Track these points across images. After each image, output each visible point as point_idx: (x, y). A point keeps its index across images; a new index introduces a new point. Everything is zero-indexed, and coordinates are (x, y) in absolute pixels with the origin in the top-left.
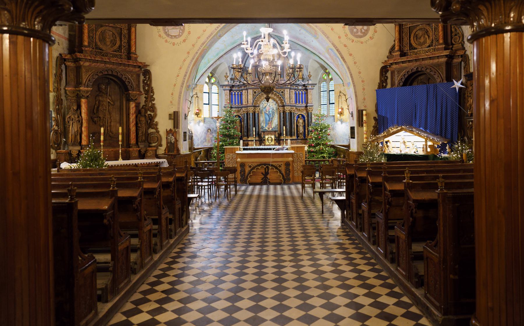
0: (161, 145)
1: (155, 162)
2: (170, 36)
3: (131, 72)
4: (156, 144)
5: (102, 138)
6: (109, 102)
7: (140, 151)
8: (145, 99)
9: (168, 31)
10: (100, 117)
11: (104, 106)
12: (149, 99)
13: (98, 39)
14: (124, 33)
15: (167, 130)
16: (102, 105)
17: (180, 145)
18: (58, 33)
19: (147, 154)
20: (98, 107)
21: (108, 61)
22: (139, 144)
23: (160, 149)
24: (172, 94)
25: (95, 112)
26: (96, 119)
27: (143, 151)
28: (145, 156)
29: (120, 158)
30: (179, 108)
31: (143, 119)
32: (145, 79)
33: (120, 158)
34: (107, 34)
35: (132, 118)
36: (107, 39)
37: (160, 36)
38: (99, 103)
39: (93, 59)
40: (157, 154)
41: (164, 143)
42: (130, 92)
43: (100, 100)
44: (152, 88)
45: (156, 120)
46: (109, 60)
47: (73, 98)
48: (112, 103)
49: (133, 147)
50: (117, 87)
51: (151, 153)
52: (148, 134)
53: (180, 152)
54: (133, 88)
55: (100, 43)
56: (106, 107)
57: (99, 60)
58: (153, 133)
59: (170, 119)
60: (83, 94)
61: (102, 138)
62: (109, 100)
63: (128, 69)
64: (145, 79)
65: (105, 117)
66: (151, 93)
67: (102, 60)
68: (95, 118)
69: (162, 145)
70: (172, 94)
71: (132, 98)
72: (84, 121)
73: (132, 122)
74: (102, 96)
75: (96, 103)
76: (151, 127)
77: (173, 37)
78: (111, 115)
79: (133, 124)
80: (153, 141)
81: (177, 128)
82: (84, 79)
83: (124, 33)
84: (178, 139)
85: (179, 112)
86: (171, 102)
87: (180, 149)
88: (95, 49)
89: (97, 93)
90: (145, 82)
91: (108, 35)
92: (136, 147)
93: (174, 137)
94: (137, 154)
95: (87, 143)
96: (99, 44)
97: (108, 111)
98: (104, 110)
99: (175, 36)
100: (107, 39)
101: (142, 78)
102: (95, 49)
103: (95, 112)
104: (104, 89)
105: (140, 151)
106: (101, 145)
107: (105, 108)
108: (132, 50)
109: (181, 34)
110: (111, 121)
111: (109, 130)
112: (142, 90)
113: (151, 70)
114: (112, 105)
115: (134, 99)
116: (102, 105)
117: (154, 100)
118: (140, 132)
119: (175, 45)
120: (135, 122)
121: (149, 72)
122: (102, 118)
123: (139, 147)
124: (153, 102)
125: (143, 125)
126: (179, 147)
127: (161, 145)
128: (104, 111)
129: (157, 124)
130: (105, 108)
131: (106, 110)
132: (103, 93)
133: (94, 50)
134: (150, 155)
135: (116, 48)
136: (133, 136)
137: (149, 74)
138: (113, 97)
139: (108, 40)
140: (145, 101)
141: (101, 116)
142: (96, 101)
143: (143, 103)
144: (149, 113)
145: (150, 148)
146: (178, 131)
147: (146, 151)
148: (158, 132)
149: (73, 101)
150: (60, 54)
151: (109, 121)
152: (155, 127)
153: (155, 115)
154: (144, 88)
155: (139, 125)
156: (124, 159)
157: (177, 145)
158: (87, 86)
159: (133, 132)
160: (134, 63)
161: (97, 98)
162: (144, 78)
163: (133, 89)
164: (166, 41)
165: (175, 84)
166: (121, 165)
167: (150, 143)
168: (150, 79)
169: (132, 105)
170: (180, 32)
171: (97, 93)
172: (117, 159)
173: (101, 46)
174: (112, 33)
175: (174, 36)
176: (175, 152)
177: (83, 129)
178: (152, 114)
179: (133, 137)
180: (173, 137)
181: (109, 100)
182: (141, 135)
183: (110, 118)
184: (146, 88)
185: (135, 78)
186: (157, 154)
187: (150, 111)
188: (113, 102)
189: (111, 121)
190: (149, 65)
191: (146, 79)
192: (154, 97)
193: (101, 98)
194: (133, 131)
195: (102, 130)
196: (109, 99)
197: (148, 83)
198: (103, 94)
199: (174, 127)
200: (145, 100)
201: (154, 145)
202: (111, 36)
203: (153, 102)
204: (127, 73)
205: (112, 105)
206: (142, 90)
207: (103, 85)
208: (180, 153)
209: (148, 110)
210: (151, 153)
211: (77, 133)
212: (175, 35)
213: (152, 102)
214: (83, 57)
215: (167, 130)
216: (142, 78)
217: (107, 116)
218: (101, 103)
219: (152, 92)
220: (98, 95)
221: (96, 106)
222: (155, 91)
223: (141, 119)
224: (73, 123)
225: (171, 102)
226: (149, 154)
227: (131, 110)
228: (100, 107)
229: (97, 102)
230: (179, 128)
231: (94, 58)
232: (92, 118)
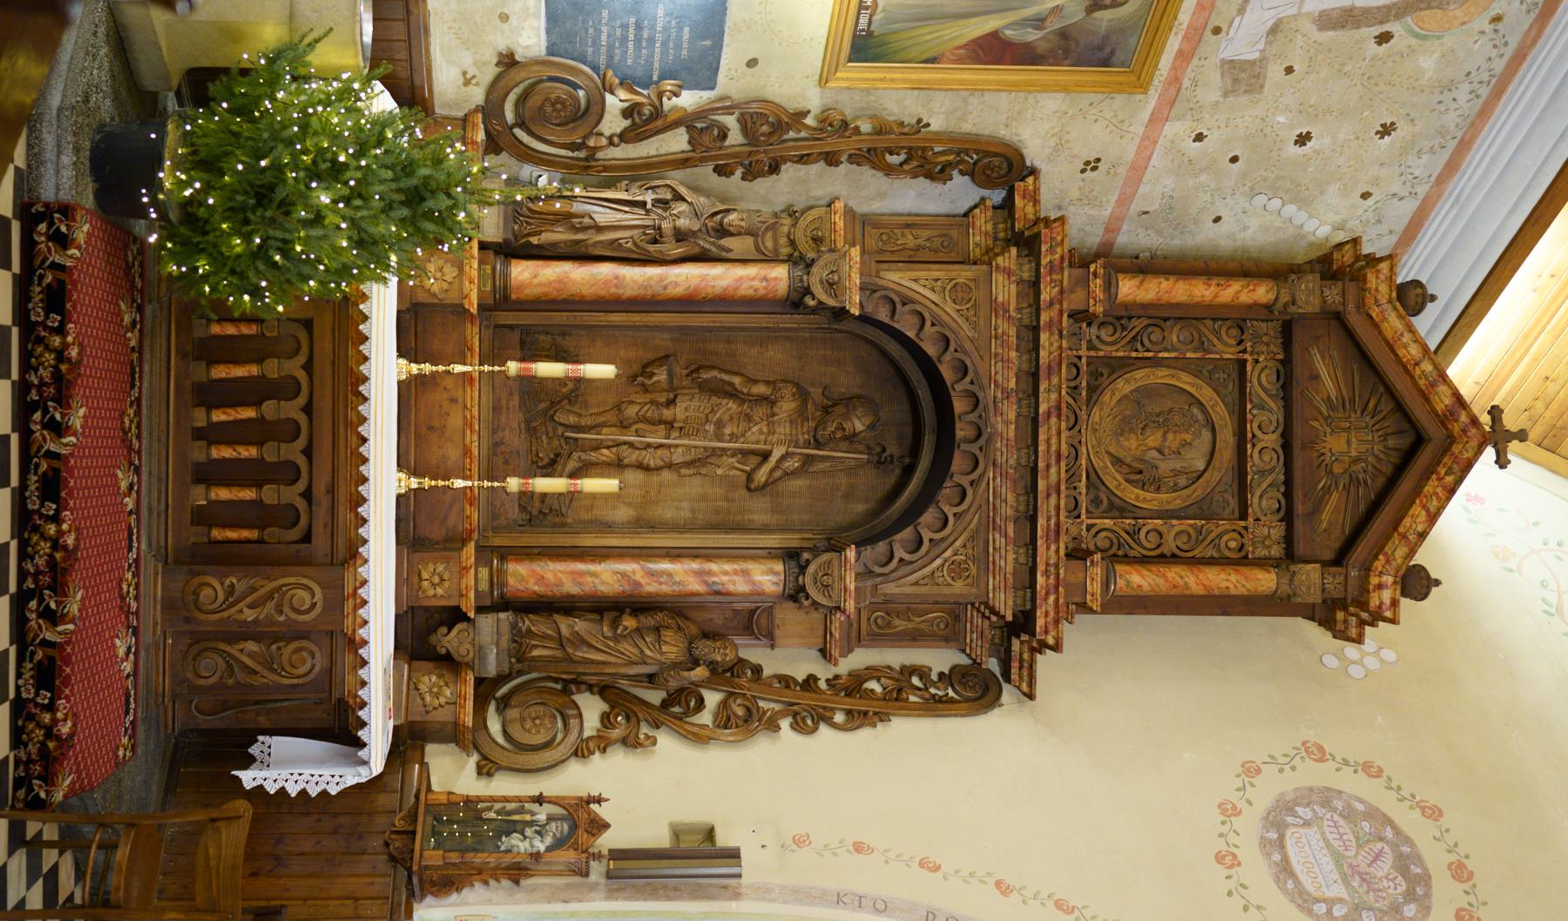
0: (486, 769)
1: (363, 705)
2: (1273, 835)
3: (984, 562)
4: (500, 739)
5: (548, 369)
6: (765, 456)
7: (455, 616)
8: (800, 677)
9: (1307, 824)
10: (671, 403)
11: (743, 425)
12: (807, 699)
13: (1153, 380)
14: (1220, 536)
15: (599, 800)
16: (748, 418)
17: (489, 902)
18: (1153, 162)
19: (430, 673)
20: (732, 394)
21: (1043, 408)
22: (502, 615)
23: (463, 767)
24: (859, 848)
25: (705, 375)
26: (661, 376)
27: (452, 640)
28: (416, 664)
29: (414, 483)
30: (764, 892)
31: (672, 648)
32: (934, 677)
33: (414, 483)
34: (1188, 437)
35: (682, 576)
36: (1159, 435)
37: (1251, 770)
38: (764, 399)
39: (1044, 317)
40: (431, 749)
41: (505, 786)
42: (851, 553)
43: (773, 403)
44: (883, 717)
45: (666, 742)
46: (1049, 414)
47: (783, 241)
48: (762, 475)
49: (484, 573)
50: (860, 508)
51: (437, 695)
52: (566, 692)
53: (429, 900)
54: (877, 570)
55: (1125, 396)
56: (733, 437)
57: (1043, 354)
58: (574, 722)
59: (677, 832)
60: (821, 263)
61: (548, 369)
62: (777, 453)
63: (1000, 541)
64: (934, 677)
65: (676, 434)
66: (849, 712)
67: (1042, 374)
68: (670, 374)
69: (489, 775)
70: (859, 848)
71: (811, 569)
72: (652, 272)
73: (651, 574)
74: (802, 413)
75: (756, 382)
76: (613, 707)
77: (1277, 857)
78: (684, 471)
79: (639, 577)
80: (522, 720)
81: (609, 875)
82: (914, 274)
83: (1220, 536)
84: (534, 889)
85: (736, 895)
86: (800, 841)
87: (454, 897)
88: (1090, 359)
89: (816, 392)
90: (915, 681)
91: (1185, 444)
92: (484, 586)
93: (549, 849)
94: (436, 588)
95: (521, 287)
96: (1123, 387)
97: (714, 452)
98: (720, 424)
99: (1285, 869)
100: (1159, 435)
101: (939, 659)
102: (1090, 359)
103: (705, 375)
104: (847, 425)
105: (455, 616)
106: (503, 364)
107: (727, 431)
108: (1128, 568)
109: (1321, 908)
110: (647, 469)
111: (593, 456)
112: (860, 658)
113: (997, 711)
114: (750, 476)
115: (807, 580)
116: (748, 418)
117: (798, 727)
118: (581, 625)
119: (1222, 871)
120: (651, 587)
121: (990, 696)
122: (667, 413)
123: (480, 610)
124: (785, 724)
125: (627, 648)
126: (465, 892)
127: (486, 769)
128: (710, 428)
129: (631, 743)
130: (727, 431)
131: (719, 438)
132: (821, 423)
133: (1083, 352)
134: (423, 688)
135: (1111, 484)
136: (559, 577)
137: (968, 700)
138: (797, 483)
139: (1154, 439)
140: (786, 681)
141: (680, 411)
142: (767, 383)
143: (772, 662)
144: (712, 698)
145: (470, 691)
146: (593, 887)
147: (449, 663)
148: (581, 752)
149: (769, 244)
150: (1033, 172)
151: (650, 458)
152: (616, 733)
153: (699, 738)
154: (874, 672)
155: (629, 622)
156: (408, 391)
157: (485, 875)
158: (867, 288)
159: (581, 574)
160: (1046, 573)
161: (788, 391)
162: (941, 675)
163: (870, 573)
164: (1229, 811)
165: (937, 868)
166: (363, 500)
167: (504, 704)
168: (935, 706)
169: (766, 578)
170: (1331, 902)
171: (816, 392)
172: (405, 350)
173: (1108, 399)
174: (1200, 465)
175: (1286, 860)
176: (430, 855)
177: (605, 270)
178: (705, 718)
179: (549, 576)
180: (549, 840)
181: (777, 453)
182: (565, 631)
183: (670, 466)
184: (873, 685)
185: (947, 591)
186: (431, 749)
187: (724, 704)
188: (766, 485)
189: (647, 469)
190: (1030, 696)
191: (934, 684)
192: (823, 728)
193: (787, 406)
194: (594, 574)
195: (602, 371)
196: (783, 458)
197: (912, 698)
198: (812, 424)
199: (617, 855)
200: (794, 679)
201: (494, 725)
202: (1178, 465)
203: (785, 724)
204: (972, 538)
205: (750, 476)
206: (860, 658)
207: (868, 421)
208: (423, 897)
209: (731, 694)
210: (437, 695)
211: (585, 229)
212: (1294, 860)
213: (783, 714)
214: (1044, 261)
215: (599, 800)
216: (939, 659)
217: (683, 447)
218: (759, 412)
219: (859, 719)
220: (802, 394)
221: (737, 380)
222: (865, 734)
223: (668, 635)
224: (643, 204)
225: (800, 841)
226: (429, 680)
227: (728, 567)
228: (733, 405)
229: (761, 389)
230: (611, 894)
231: (1050, 324)
232: (667, 357)
